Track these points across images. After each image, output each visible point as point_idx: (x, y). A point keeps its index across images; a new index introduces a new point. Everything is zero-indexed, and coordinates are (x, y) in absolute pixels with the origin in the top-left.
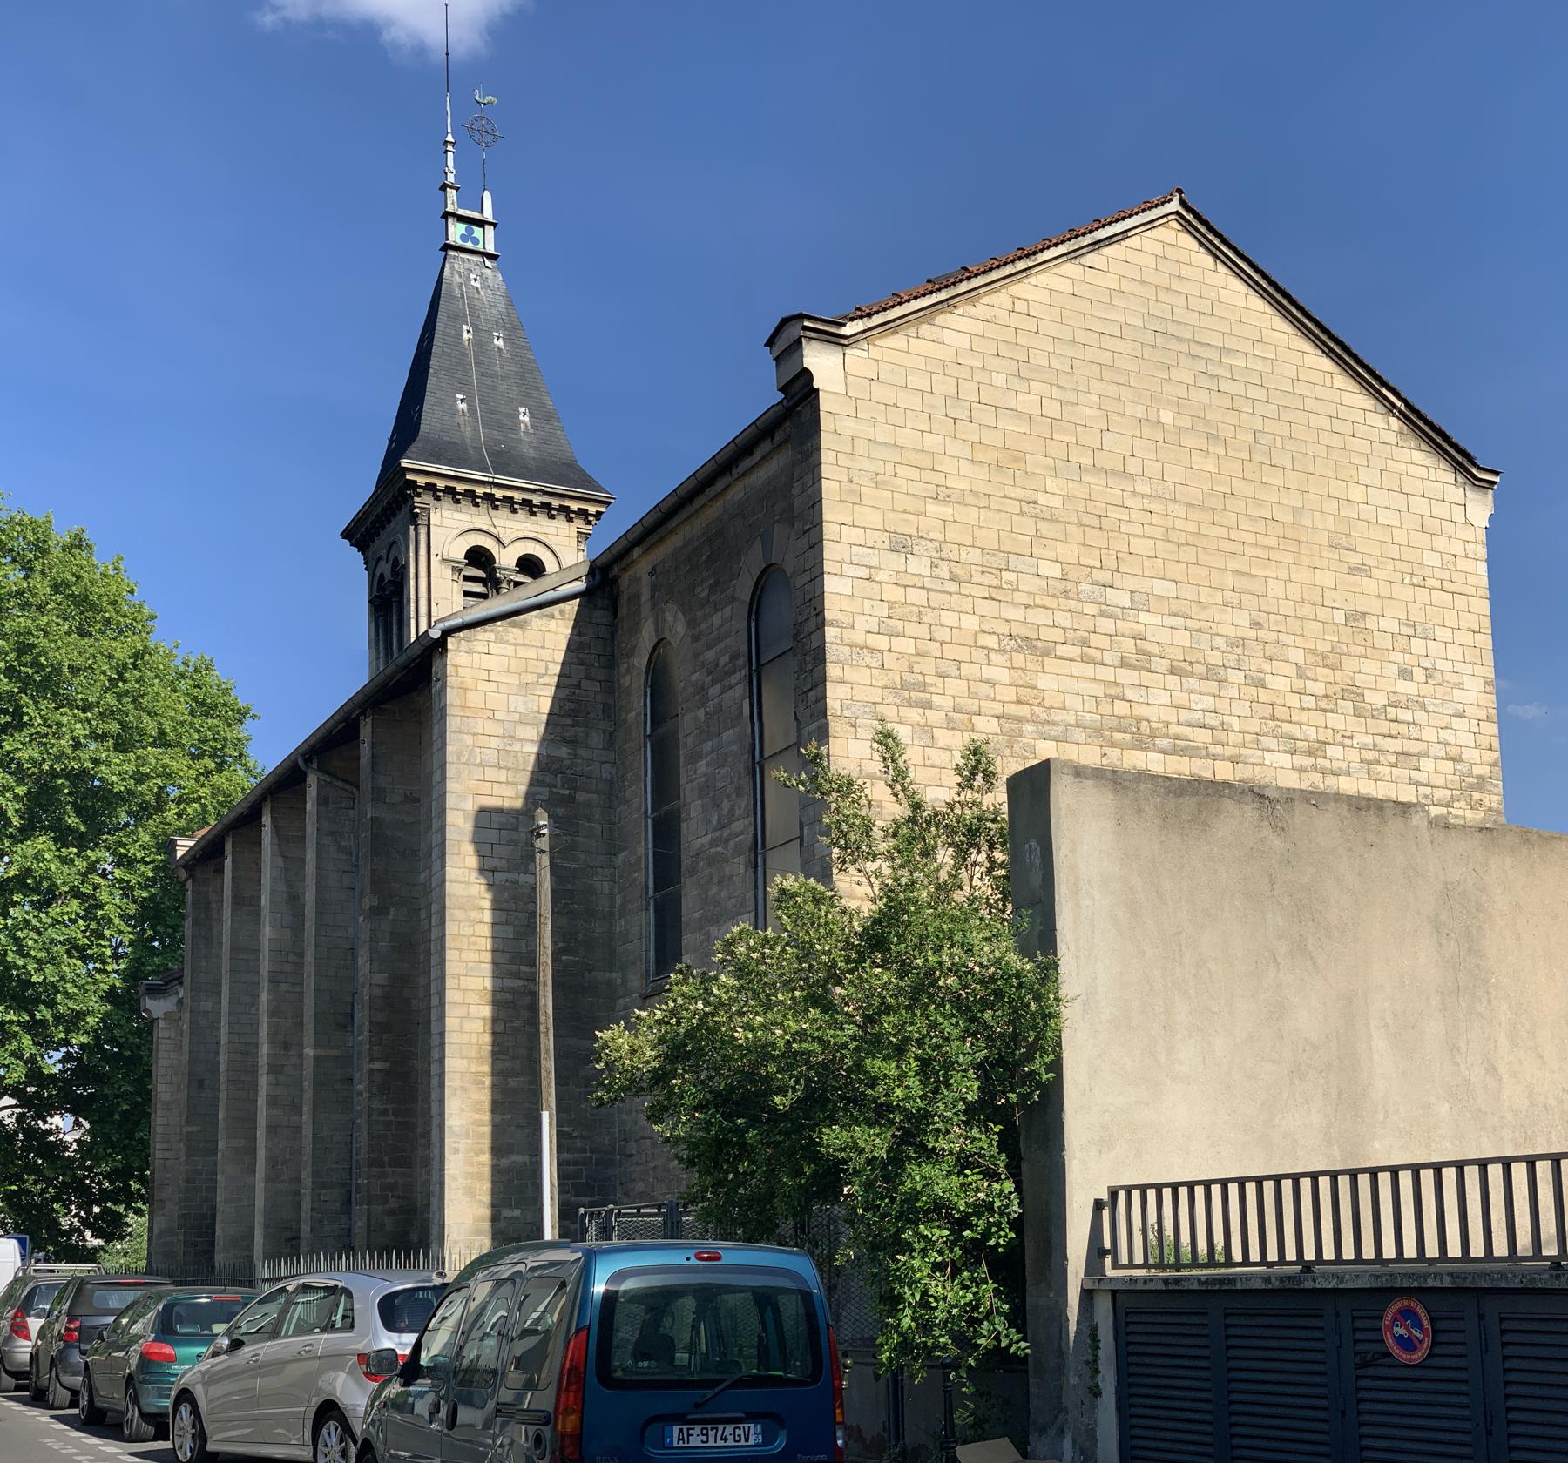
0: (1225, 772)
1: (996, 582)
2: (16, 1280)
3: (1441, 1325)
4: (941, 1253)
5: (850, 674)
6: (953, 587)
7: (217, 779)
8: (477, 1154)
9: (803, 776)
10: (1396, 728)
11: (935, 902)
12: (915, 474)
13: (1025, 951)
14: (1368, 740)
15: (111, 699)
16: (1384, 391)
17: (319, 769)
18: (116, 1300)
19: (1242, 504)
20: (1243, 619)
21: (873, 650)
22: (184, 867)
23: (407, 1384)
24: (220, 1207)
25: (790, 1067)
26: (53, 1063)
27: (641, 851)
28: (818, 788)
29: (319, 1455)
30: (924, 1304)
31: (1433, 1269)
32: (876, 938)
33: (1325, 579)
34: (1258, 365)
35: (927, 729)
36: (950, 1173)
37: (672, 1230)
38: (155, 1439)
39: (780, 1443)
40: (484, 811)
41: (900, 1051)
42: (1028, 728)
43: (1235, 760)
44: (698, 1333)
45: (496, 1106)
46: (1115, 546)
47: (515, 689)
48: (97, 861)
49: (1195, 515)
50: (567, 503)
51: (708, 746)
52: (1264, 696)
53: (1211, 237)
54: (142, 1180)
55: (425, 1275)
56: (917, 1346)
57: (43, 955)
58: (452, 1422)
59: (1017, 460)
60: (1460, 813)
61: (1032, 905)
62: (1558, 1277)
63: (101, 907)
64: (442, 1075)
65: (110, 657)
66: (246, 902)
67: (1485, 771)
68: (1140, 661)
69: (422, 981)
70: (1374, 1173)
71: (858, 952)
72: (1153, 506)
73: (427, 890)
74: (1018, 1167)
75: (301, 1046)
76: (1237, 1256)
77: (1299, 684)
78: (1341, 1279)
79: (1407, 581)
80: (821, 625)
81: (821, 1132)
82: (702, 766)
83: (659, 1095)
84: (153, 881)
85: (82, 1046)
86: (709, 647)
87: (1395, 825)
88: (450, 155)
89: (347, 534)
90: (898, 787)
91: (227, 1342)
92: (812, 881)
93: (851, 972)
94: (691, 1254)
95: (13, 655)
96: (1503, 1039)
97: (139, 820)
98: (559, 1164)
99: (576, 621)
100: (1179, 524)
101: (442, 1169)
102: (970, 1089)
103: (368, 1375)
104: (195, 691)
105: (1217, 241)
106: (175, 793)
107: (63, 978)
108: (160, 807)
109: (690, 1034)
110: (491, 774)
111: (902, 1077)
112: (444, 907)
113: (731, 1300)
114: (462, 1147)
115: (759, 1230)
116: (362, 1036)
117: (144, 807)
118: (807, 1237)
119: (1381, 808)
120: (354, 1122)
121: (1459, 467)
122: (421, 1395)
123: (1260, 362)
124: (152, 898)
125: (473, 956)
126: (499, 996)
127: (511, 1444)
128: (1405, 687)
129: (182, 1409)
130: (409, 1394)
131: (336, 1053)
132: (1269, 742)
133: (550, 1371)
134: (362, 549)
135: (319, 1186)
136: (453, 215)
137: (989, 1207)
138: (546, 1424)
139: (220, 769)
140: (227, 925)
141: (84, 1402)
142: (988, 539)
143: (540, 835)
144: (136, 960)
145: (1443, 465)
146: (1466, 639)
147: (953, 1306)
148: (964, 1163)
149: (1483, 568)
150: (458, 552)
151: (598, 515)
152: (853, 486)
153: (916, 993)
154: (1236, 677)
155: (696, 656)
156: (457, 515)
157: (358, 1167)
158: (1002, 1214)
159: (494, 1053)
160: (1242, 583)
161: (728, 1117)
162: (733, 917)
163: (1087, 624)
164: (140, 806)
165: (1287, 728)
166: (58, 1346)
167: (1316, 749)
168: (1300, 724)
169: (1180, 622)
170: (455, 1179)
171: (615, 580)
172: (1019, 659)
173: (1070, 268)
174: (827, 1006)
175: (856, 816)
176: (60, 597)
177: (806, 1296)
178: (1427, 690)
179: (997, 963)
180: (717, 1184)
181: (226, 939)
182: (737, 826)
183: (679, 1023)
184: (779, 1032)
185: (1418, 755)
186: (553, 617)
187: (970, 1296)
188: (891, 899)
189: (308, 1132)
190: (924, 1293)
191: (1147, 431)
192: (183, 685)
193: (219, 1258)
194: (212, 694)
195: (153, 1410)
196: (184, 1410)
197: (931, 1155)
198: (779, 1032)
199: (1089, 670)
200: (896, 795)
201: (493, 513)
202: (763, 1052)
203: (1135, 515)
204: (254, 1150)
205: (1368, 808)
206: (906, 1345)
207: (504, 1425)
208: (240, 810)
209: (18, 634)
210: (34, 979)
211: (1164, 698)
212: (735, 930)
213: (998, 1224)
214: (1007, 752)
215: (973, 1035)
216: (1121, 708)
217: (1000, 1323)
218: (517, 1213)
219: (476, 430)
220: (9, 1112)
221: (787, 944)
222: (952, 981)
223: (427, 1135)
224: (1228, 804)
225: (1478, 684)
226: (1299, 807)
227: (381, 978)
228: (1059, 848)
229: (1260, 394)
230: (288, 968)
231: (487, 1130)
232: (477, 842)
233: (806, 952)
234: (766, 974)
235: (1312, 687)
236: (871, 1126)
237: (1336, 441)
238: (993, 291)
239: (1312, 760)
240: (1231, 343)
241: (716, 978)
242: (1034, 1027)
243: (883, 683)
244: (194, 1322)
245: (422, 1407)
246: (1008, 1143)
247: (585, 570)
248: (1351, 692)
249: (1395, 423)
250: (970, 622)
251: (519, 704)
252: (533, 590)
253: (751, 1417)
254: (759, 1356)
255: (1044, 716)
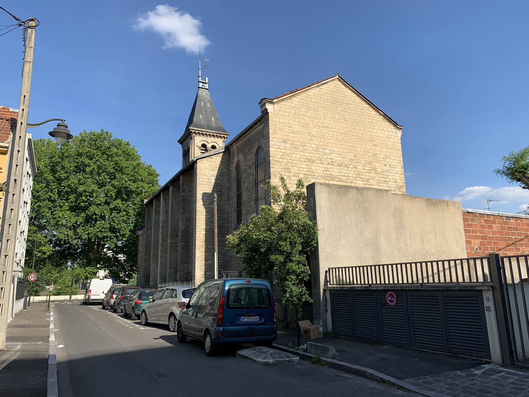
0: (349, 184)
1: (303, 149)
2: (111, 287)
3: (398, 297)
4: (294, 281)
5: (275, 166)
6: (295, 149)
7: (152, 188)
8: (202, 261)
9: (266, 186)
10: (383, 176)
11: (293, 210)
12: (287, 128)
13: (310, 220)
14: (378, 178)
15: (133, 173)
16: (379, 111)
17: (172, 186)
18: (131, 291)
19: (351, 133)
20: (352, 155)
21: (279, 162)
22: (146, 205)
23: (187, 309)
24: (151, 273)
25: (264, 243)
26: (120, 244)
27: (234, 200)
28: (269, 188)
29: (170, 323)
30: (291, 292)
31: (396, 286)
32: (281, 217)
33: (369, 147)
34: (354, 107)
35: (290, 177)
36: (296, 265)
37: (240, 276)
38: (138, 320)
39: (263, 321)
40: (204, 193)
41: (285, 240)
42: (310, 177)
43: (351, 183)
44: (246, 297)
45: (206, 252)
46: (326, 141)
47: (210, 170)
48: (129, 204)
49: (342, 135)
50: (221, 135)
51: (247, 180)
52: (357, 170)
53: (344, 82)
54: (136, 267)
55: (191, 286)
56: (290, 300)
57: (118, 223)
58: (196, 317)
59: (307, 125)
60: (397, 192)
61: (312, 211)
62: (422, 287)
63: (129, 213)
64: (195, 245)
65: (132, 165)
66: (157, 212)
67: (402, 184)
68: (332, 163)
69: (192, 227)
70: (383, 266)
71: (277, 220)
72: (334, 134)
73: (193, 209)
74: (310, 264)
75: (168, 240)
76: (355, 283)
77: (364, 168)
78: (377, 288)
79: (385, 147)
80: (269, 157)
81: (270, 256)
82: (246, 184)
83: (238, 248)
84: (139, 208)
85: (125, 241)
86: (248, 162)
87: (385, 194)
88: (200, 71)
89: (178, 142)
90: (285, 188)
91: (152, 300)
92: (268, 206)
93: (276, 224)
94: (245, 281)
95: (114, 165)
96: (408, 238)
97: (137, 196)
98: (218, 263)
99: (222, 157)
100: (339, 137)
101: (195, 264)
102: (300, 248)
103: (180, 307)
104: (148, 171)
105: (346, 83)
106: (144, 191)
107: (122, 227)
108: (141, 193)
109: (244, 236)
110: (206, 186)
111: (286, 245)
112: (196, 212)
113: (253, 290)
114: (199, 260)
115: (258, 276)
116: (179, 238)
117: (138, 194)
118: (267, 278)
119: (382, 191)
120: (178, 255)
121: (394, 125)
122: (190, 311)
123: (355, 106)
124: (139, 211)
125: (202, 222)
126: (207, 230)
127: (208, 320)
128: (385, 168)
129: (143, 313)
130: (188, 311)
131: (174, 241)
132: (358, 179)
133: (216, 306)
134: (181, 144)
135: (171, 268)
136: (200, 82)
137: (304, 272)
138: (216, 316)
139: (153, 186)
140: (154, 216)
141: (124, 312)
142: (302, 140)
143: (215, 198)
144: (136, 223)
145: (391, 125)
146: (397, 158)
147: (297, 292)
148: (299, 263)
149: (400, 145)
150: (200, 145)
151: (227, 137)
152: (275, 131)
153: (289, 228)
154: (351, 166)
155: (245, 163)
156: (200, 138)
157: (178, 264)
158: (307, 273)
159: (205, 241)
160: (352, 148)
161: (252, 253)
162: (252, 213)
163: (321, 156)
164: (137, 193)
165: (361, 176)
166: (119, 301)
167: (368, 181)
168: (364, 175)
169: (340, 156)
170: (197, 266)
171: (230, 149)
172: (308, 163)
173: (317, 89)
174: (271, 231)
175: (276, 193)
176: (124, 154)
177: (268, 290)
178: (389, 169)
179: (305, 222)
180: (249, 267)
181: (153, 219)
182: (253, 195)
183: (242, 234)
184: (262, 236)
185: (388, 181)
186: (218, 156)
187: (300, 290)
188: (284, 210)
189: (168, 257)
190: (291, 290)
191: (332, 119)
192: (146, 170)
193: (150, 283)
194: (152, 172)
195: (137, 314)
196: (143, 314)
197: (291, 261)
198: (262, 236)
199: (322, 165)
200: (284, 189)
201: (207, 137)
202: (258, 240)
203: (330, 135)
204: (158, 261)
205: (379, 191)
206: (287, 300)
207: (207, 317)
208: (156, 194)
209: (115, 161)
210: (116, 227)
211: (337, 171)
212: (253, 216)
213: (306, 275)
214: (305, 181)
215: (300, 237)
216: (328, 173)
217: (307, 296)
218: (210, 273)
219: (204, 122)
220: (110, 254)
221: (263, 219)
222: (296, 226)
223: (192, 257)
224: (351, 190)
225: (400, 167)
226: (365, 191)
227: (184, 226)
228: (317, 200)
229: (355, 112)
230: (165, 225)
231: (204, 256)
232: (203, 199)
233: (267, 220)
234: (259, 224)
235: (366, 168)
236: (280, 255)
237: (370, 121)
238: (302, 93)
239: (367, 182)
240: (349, 102)
241: (249, 225)
242: (313, 235)
243: (282, 168)
244: (145, 296)
245: (190, 314)
246: (308, 259)
247: (224, 147)
248: (374, 169)
249: (381, 117)
250: (298, 156)
251: (211, 173)
252: (213, 151)
253: (257, 315)
254: (259, 302)
255: (313, 174)
